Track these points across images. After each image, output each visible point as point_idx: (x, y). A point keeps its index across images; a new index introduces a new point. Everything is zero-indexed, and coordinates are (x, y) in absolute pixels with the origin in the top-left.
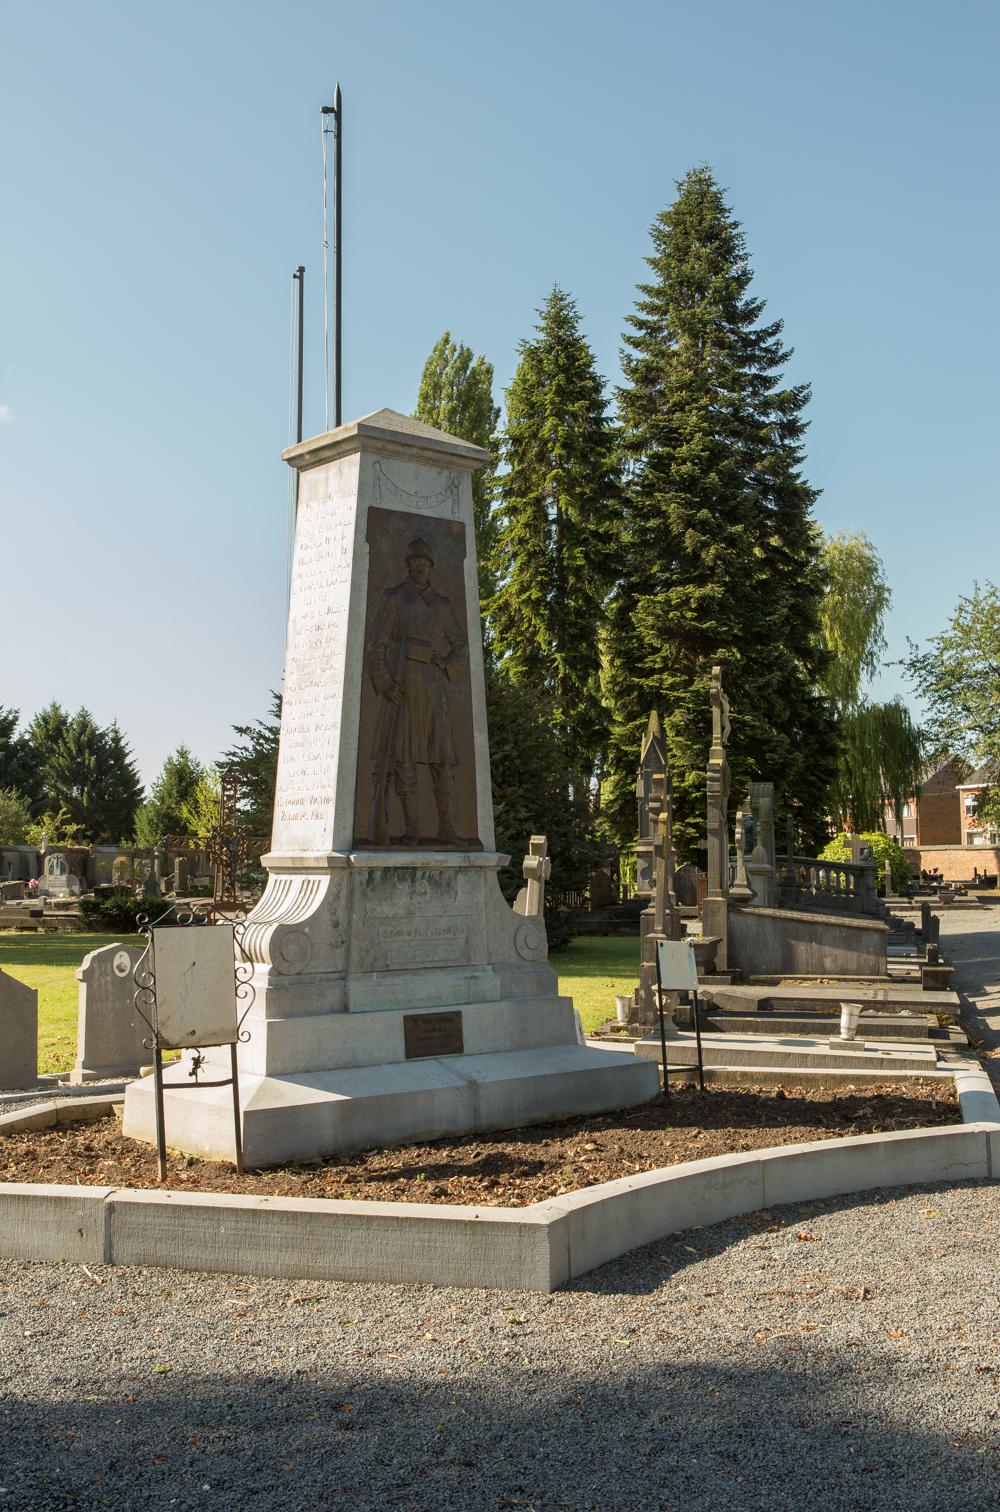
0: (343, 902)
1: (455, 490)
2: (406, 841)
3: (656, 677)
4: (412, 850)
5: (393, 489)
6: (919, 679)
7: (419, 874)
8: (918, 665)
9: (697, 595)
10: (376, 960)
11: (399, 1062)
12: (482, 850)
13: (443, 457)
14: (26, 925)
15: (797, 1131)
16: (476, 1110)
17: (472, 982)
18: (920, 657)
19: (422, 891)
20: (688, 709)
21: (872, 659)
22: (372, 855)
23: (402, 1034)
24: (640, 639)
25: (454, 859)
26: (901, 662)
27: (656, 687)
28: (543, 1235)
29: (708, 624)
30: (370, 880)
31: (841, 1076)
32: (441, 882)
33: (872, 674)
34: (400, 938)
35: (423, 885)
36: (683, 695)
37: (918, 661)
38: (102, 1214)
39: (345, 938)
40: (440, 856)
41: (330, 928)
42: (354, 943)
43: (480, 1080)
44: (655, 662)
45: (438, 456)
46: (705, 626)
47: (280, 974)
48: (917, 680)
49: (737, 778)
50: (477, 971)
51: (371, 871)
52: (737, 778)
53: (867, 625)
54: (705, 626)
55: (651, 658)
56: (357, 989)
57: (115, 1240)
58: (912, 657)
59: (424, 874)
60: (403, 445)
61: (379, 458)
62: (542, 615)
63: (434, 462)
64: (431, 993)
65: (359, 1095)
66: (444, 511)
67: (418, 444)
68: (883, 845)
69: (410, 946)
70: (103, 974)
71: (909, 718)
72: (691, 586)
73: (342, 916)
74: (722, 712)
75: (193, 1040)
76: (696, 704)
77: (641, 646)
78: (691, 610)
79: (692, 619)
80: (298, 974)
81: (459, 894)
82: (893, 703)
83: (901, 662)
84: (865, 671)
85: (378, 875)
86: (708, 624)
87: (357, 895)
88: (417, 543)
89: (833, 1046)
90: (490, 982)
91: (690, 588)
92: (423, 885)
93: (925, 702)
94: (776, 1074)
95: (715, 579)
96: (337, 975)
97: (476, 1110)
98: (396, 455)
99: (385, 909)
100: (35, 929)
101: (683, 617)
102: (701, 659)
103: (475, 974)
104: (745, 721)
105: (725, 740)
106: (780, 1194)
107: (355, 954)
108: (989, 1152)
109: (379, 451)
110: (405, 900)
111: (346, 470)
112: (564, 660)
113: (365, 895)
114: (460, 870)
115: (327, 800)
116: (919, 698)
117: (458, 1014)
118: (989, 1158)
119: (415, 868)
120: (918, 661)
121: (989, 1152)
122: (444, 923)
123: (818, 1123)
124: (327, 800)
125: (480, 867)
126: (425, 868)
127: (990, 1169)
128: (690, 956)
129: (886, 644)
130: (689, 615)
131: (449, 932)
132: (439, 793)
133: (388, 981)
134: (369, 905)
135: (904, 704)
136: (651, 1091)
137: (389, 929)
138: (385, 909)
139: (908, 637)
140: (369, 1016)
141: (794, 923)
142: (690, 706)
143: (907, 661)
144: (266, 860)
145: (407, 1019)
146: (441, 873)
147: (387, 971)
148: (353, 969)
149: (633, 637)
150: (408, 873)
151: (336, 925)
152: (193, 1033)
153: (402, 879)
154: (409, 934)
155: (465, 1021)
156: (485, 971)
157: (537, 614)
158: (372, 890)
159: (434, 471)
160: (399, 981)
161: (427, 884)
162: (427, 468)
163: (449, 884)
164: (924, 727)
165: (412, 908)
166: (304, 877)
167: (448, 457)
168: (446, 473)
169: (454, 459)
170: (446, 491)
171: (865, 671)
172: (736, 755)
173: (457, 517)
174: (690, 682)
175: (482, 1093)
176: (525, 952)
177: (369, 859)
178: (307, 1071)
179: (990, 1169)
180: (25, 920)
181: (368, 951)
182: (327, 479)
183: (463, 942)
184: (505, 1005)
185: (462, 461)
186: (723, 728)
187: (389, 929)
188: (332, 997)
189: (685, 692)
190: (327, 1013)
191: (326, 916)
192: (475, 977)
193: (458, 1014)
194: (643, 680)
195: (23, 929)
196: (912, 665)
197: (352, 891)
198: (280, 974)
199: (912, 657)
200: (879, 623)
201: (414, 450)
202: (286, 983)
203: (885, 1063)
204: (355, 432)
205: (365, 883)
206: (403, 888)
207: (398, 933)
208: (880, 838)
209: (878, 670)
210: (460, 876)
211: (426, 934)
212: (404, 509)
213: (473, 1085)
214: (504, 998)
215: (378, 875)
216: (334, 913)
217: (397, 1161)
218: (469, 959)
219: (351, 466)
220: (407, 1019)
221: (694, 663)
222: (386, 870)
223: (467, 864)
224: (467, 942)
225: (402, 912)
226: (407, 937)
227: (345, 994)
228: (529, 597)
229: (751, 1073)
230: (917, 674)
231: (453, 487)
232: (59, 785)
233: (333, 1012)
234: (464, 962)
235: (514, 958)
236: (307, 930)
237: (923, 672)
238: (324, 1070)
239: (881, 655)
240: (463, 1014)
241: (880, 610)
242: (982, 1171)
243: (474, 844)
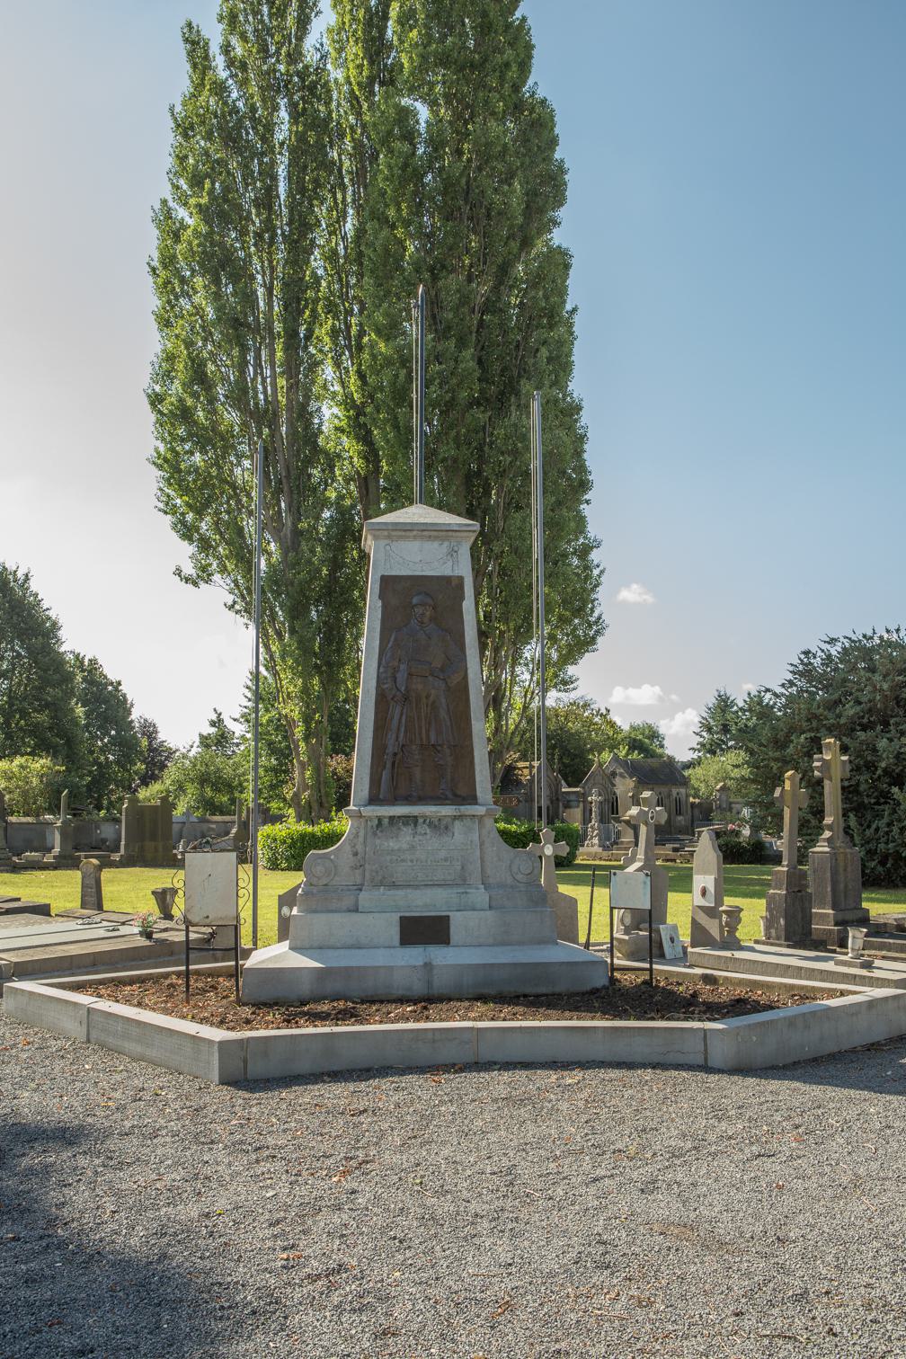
0: (361, 839)
1: (455, 554)
5: (401, 561)
7: (421, 820)
10: (384, 878)
11: (394, 947)
12: (476, 804)
13: (441, 533)
14: (668, 858)
15: (567, 1014)
16: (429, 983)
17: (462, 896)
19: (423, 832)
22: (378, 808)
23: (398, 929)
25: (447, 810)
28: (216, 1047)
31: (790, 985)
32: (440, 827)
34: (404, 864)
35: (422, 828)
39: (362, 863)
41: (351, 856)
43: (434, 963)
45: (435, 533)
47: (311, 885)
50: (469, 888)
51: (380, 819)
59: (425, 821)
60: (405, 531)
61: (387, 542)
63: (436, 538)
64: (425, 902)
65: (335, 964)
66: (446, 570)
67: (416, 528)
69: (413, 870)
80: (326, 885)
81: (456, 834)
85: (386, 821)
89: (838, 963)
90: (480, 896)
92: (422, 828)
94: (747, 980)
96: (355, 887)
97: (429, 983)
98: (400, 537)
99: (391, 844)
100: (674, 860)
103: (468, 891)
106: (486, 1054)
107: (367, 874)
108: (706, 1045)
109: (389, 537)
110: (408, 838)
113: (375, 834)
114: (455, 818)
118: (706, 1050)
119: (416, 817)
121: (706, 1045)
122: (443, 854)
123: (549, 1006)
125: (474, 816)
126: (425, 818)
127: (706, 1059)
128: (645, 883)
131: (446, 860)
133: (392, 892)
134: (378, 842)
136: (601, 981)
137: (395, 858)
138: (392, 844)
140: (371, 916)
145: (401, 917)
146: (439, 820)
147: (394, 886)
150: (412, 820)
151: (356, 854)
152: (208, 917)
154: (412, 861)
155: (452, 922)
156: (477, 889)
158: (382, 831)
159: (436, 544)
160: (401, 893)
161: (427, 827)
162: (430, 542)
163: (446, 828)
165: (414, 844)
167: (444, 533)
168: (446, 544)
169: (450, 533)
170: (447, 556)
173: (456, 573)
175: (435, 972)
177: (373, 811)
178: (321, 948)
179: (706, 1059)
180: (669, 854)
181: (377, 872)
183: (459, 868)
184: (488, 913)
185: (458, 534)
187: (395, 858)
188: (348, 902)
190: (345, 912)
192: (466, 893)
195: (667, 860)
198: (311, 885)
201: (415, 533)
202: (315, 891)
203: (857, 978)
205: (375, 826)
207: (403, 861)
210: (457, 822)
211: (426, 861)
212: (410, 573)
213: (428, 966)
215: (386, 821)
216: (354, 847)
217: (325, 1007)
218: (465, 880)
220: (401, 917)
222: (392, 818)
223: (459, 814)
224: (463, 868)
226: (410, 864)
227: (357, 901)
229: (731, 978)
231: (453, 553)
234: (462, 881)
236: (332, 857)
238: (333, 948)
240: (451, 918)
242: (701, 1061)
243: (473, 800)
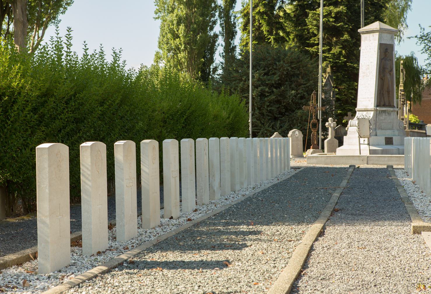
0: (375, 116)
2: (384, 106)
3: (316, 47)
4: (385, 107)
6: (424, 45)
8: (424, 38)
9: (335, 11)
18: (425, 33)
20: (330, 61)
21: (400, 34)
24: (308, 30)
25: (391, 109)
26: (416, 37)
27: (316, 52)
29: (339, 24)
30: (379, 113)
32: (389, 113)
33: (400, 41)
36: (328, 55)
37: (424, 36)
38: (366, 158)
40: (390, 109)
42: (377, 124)
44: (315, 40)
46: (338, 25)
48: (423, 45)
49: (350, 91)
52: (350, 91)
53: (400, 18)
54: (338, 25)
55: (313, 38)
56: (379, 132)
57: (368, 162)
58: (421, 34)
62: (265, 19)
63: (389, 33)
64: (389, 133)
68: (414, 120)
70: (294, 136)
71: (417, 63)
72: (332, 6)
73: (375, 119)
74: (403, 74)
75: (364, 137)
76: (333, 59)
77: (309, 33)
78: (332, 17)
79: (332, 22)
82: (410, 56)
83: (416, 37)
84: (396, 40)
85: (380, 112)
86: (339, 24)
87: (378, 115)
88: (387, 49)
91: (332, 8)
92: (387, 114)
93: (426, 56)
95: (343, 3)
101: (329, 21)
102: (335, 39)
104: (354, 66)
105: (404, 82)
107: (377, 126)
111: (375, 36)
112: (274, 39)
115: (372, 98)
116: (423, 53)
117: (392, 138)
119: (386, 111)
120: (424, 36)
122: (389, 121)
124: (372, 98)
126: (387, 111)
129: (407, 26)
130: (331, 20)
132: (389, 97)
135: (415, 56)
138: (381, 118)
139: (420, 25)
141: (423, 134)
142: (331, 60)
143: (419, 36)
144: (356, 109)
145: (385, 138)
147: (382, 129)
148: (377, 128)
149: (305, 29)
151: (374, 120)
153: (384, 113)
157: (263, 18)
159: (389, 34)
164: (424, 67)
166: (366, 112)
171: (396, 40)
172: (349, 81)
174: (330, 50)
176: (401, 127)
182: (369, 37)
186: (403, 79)
189: (329, 54)
191: (373, 119)
193: (392, 138)
194: (310, 48)
196: (421, 38)
197: (377, 114)
199: (421, 34)
200: (405, 16)
204: (379, 29)
206: (384, 114)
208: (413, 117)
209: (403, 39)
213: (398, 149)
214: (399, 135)
215: (380, 112)
219: (377, 35)
220: (385, 138)
221: (331, 41)
225: (384, 119)
228: (259, 11)
230: (423, 42)
232: (244, 95)
233: (374, 136)
235: (399, 128)
237: (426, 41)
239: (404, 31)
241: (406, 11)
